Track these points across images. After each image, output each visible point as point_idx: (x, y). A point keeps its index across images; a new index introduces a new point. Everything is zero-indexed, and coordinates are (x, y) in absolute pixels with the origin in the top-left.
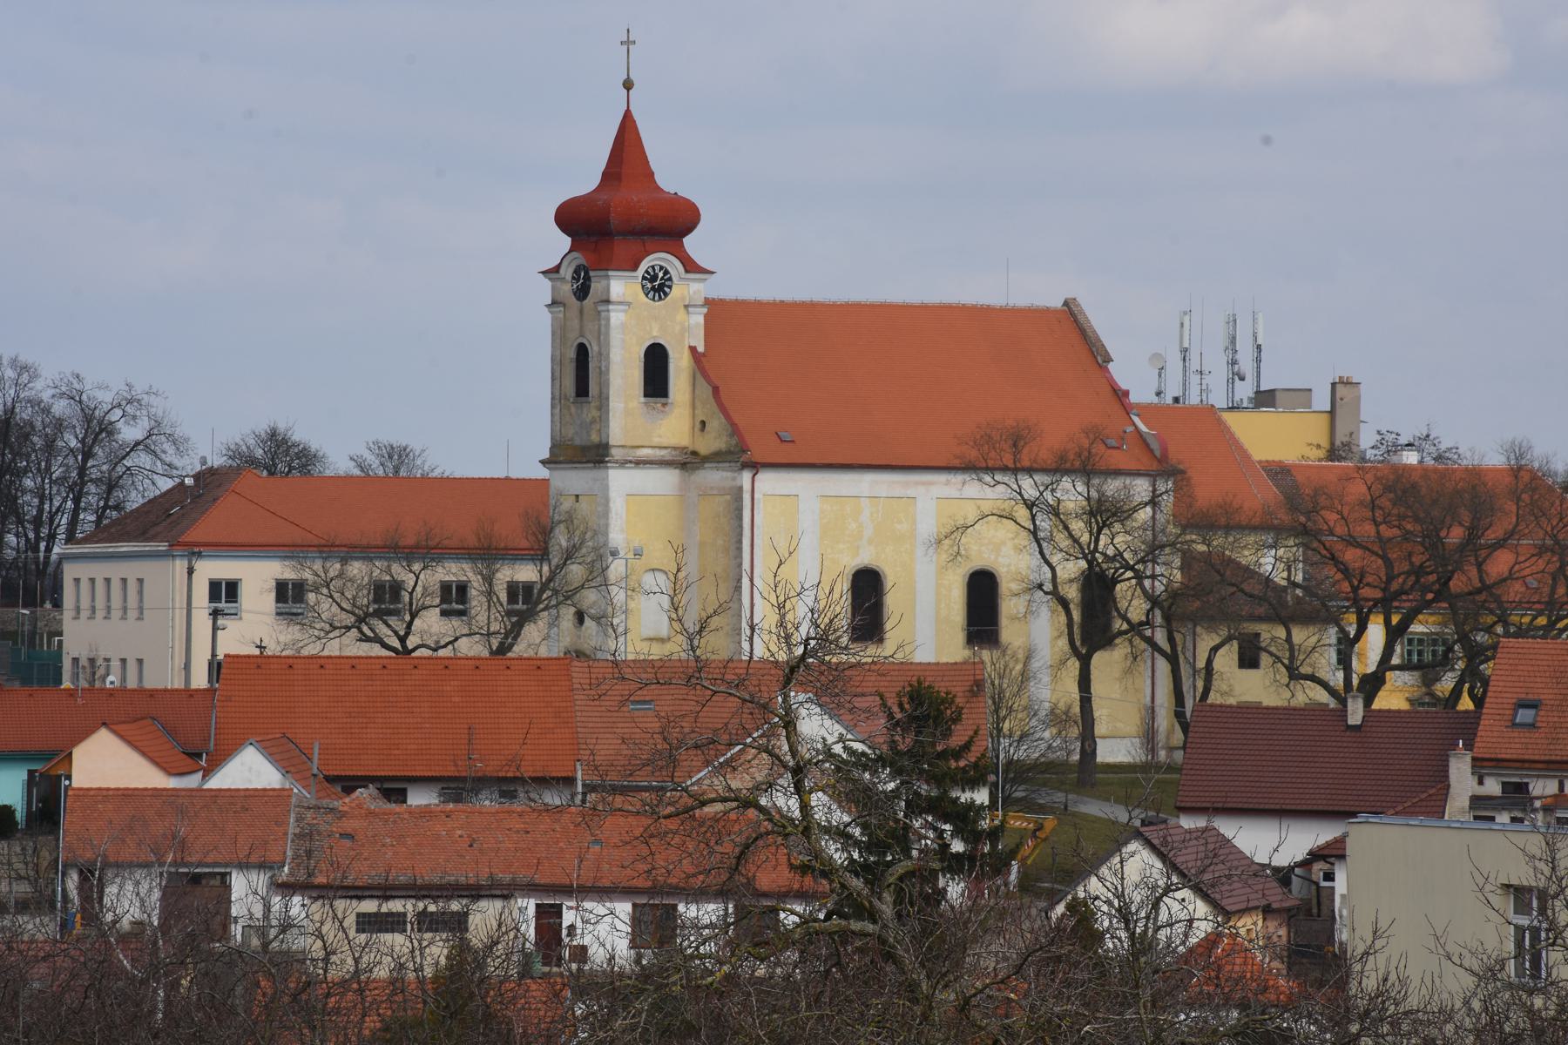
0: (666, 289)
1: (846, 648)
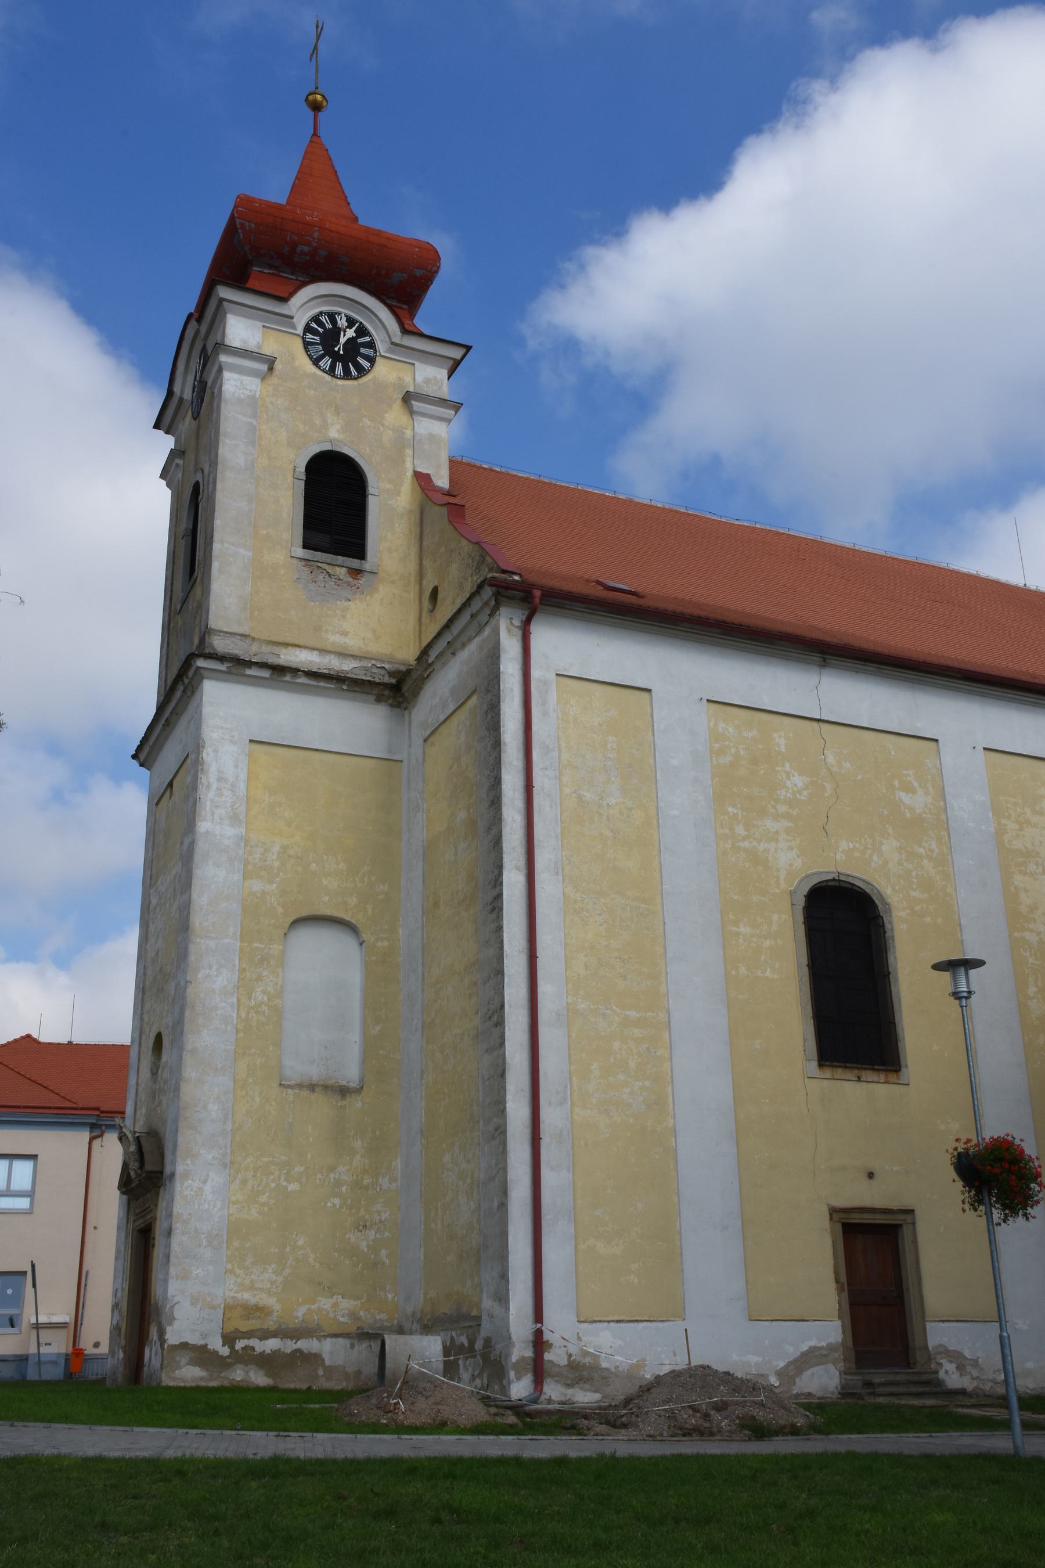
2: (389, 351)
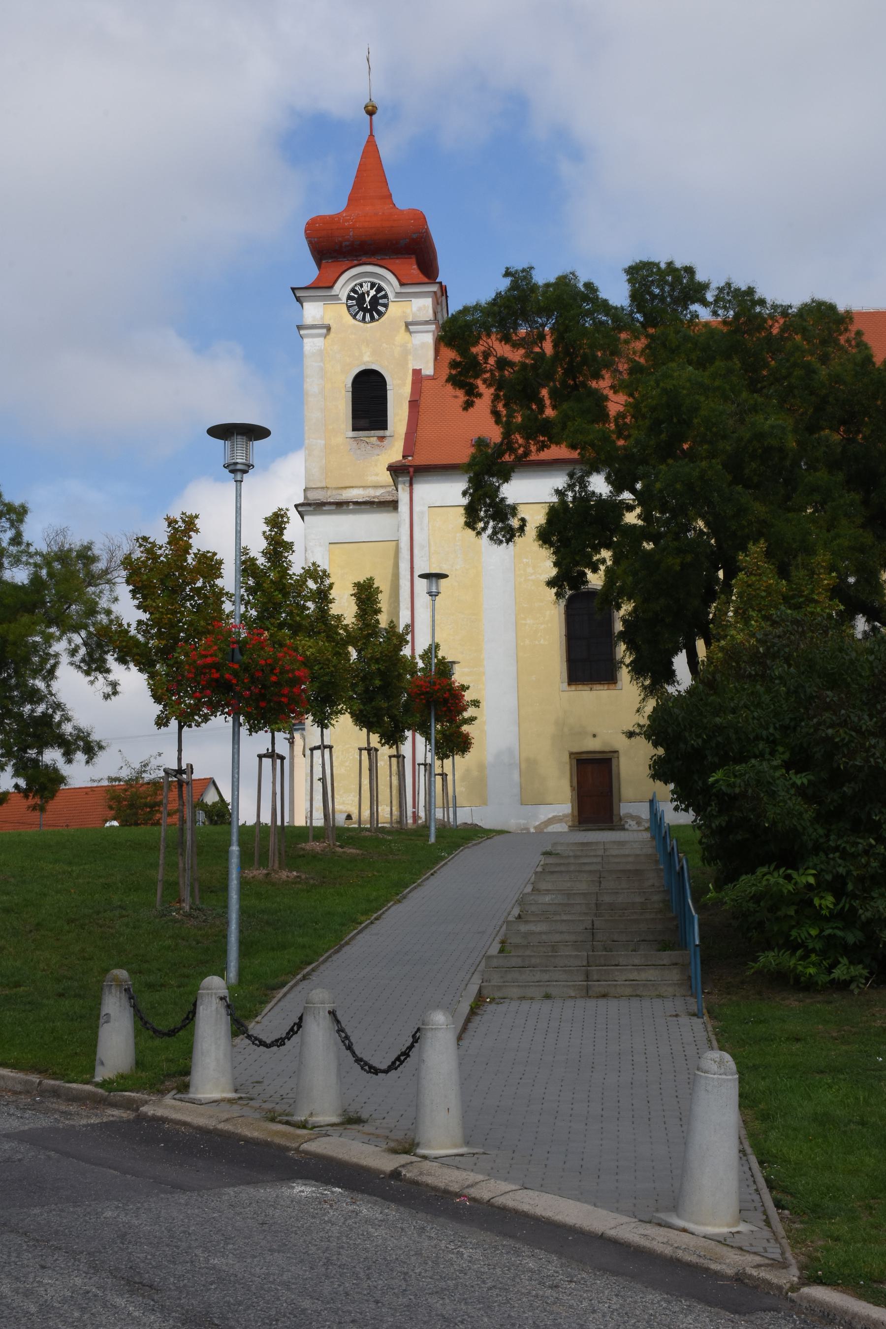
0: (380, 308)
2: (396, 297)
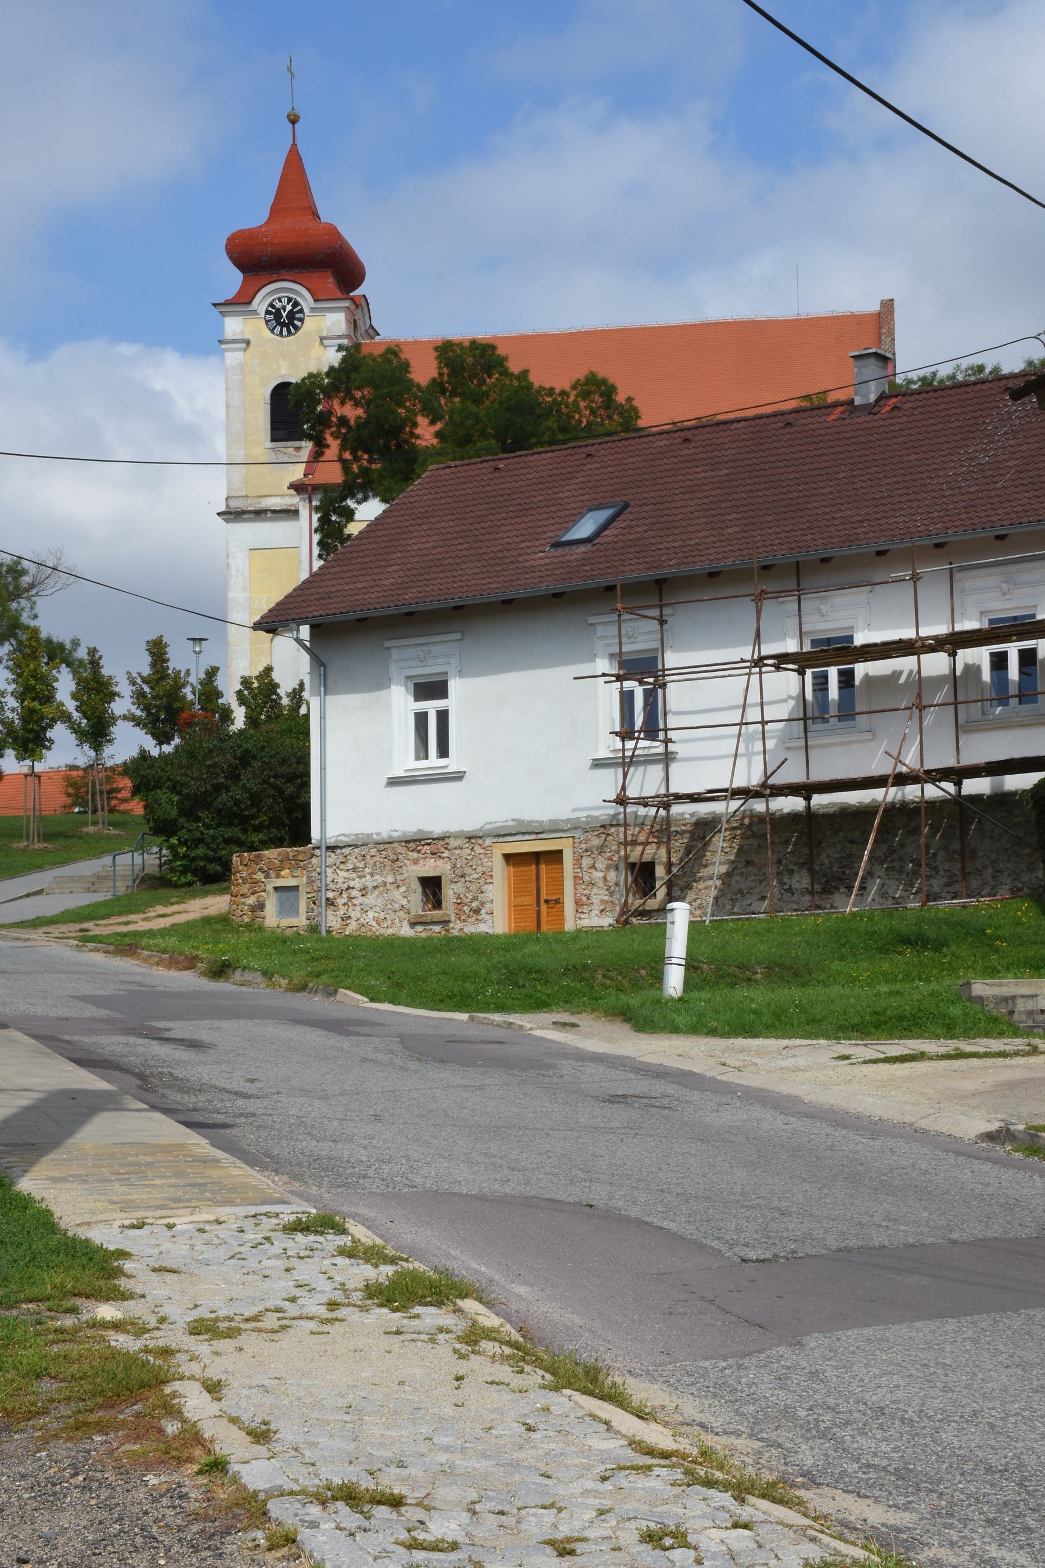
0: (296, 322)
1: (169, 779)
